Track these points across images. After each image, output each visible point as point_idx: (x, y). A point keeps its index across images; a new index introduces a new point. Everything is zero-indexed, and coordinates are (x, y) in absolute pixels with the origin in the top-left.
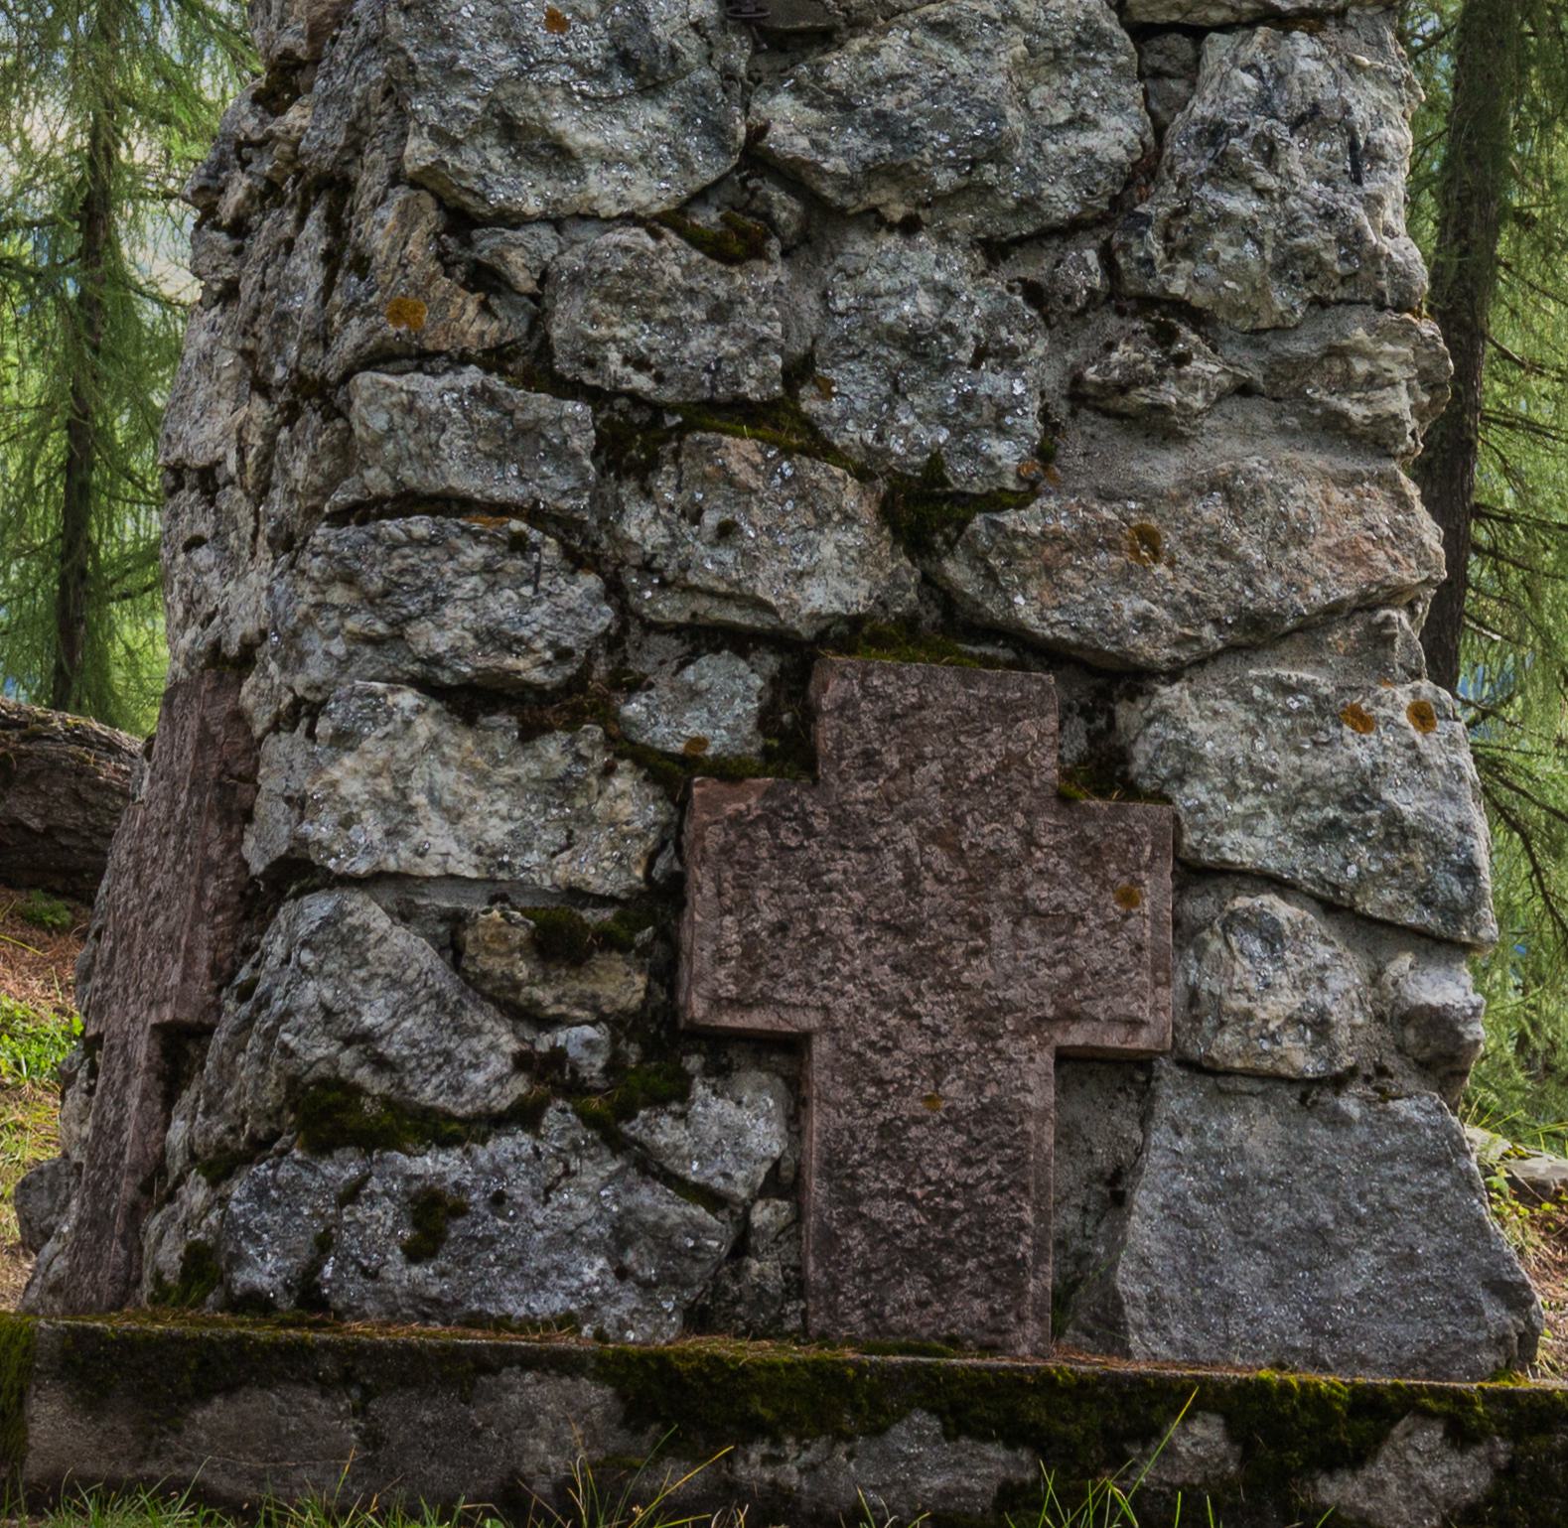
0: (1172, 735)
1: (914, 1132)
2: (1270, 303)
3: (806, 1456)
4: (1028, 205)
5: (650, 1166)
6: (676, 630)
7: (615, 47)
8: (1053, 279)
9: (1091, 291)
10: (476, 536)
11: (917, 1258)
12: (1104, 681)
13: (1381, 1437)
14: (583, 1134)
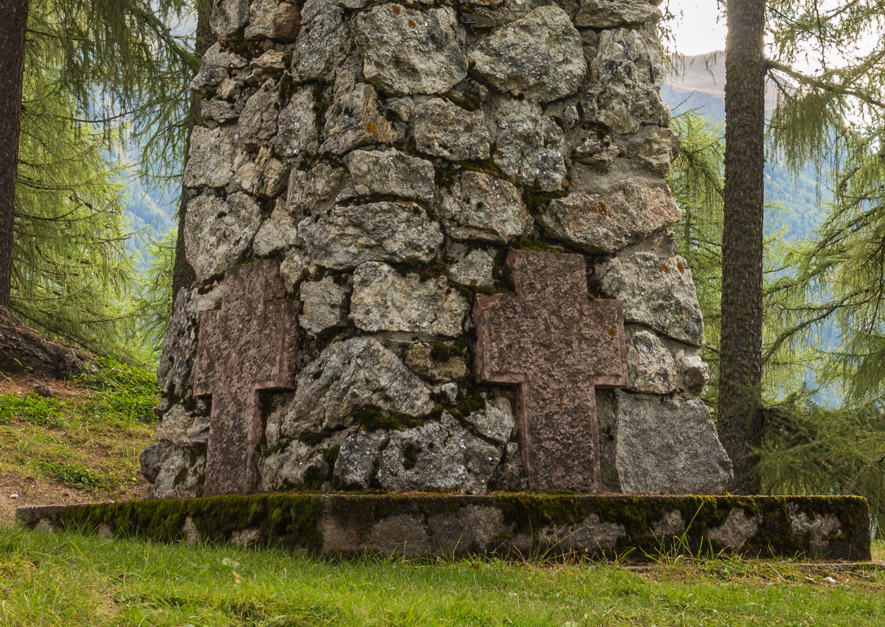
0: (616, 276)
1: (555, 417)
2: (629, 125)
3: (560, 531)
4: (555, 90)
5: (474, 432)
6: (463, 241)
7: (429, 33)
8: (564, 116)
9: (576, 120)
10: (404, 209)
11: (561, 461)
12: (595, 256)
13: (726, 515)
14: (454, 421)
